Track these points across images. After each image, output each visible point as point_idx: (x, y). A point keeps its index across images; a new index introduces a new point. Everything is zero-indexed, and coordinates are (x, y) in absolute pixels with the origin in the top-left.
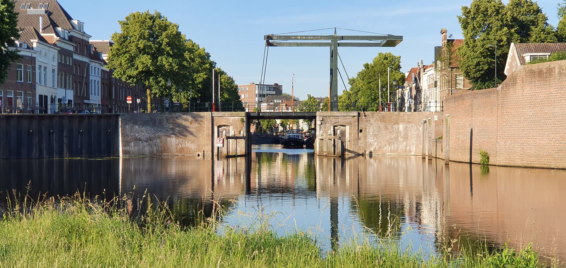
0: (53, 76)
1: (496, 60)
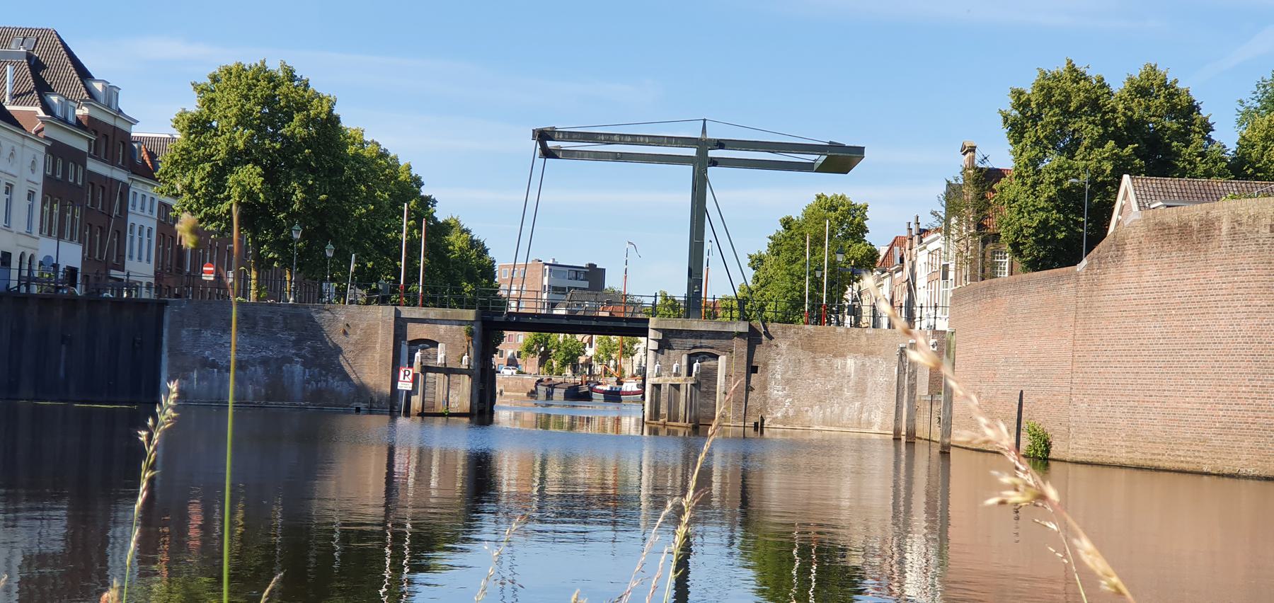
0: (31, 208)
1: (1085, 220)
